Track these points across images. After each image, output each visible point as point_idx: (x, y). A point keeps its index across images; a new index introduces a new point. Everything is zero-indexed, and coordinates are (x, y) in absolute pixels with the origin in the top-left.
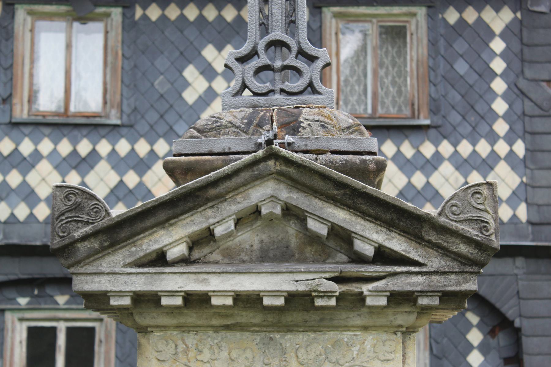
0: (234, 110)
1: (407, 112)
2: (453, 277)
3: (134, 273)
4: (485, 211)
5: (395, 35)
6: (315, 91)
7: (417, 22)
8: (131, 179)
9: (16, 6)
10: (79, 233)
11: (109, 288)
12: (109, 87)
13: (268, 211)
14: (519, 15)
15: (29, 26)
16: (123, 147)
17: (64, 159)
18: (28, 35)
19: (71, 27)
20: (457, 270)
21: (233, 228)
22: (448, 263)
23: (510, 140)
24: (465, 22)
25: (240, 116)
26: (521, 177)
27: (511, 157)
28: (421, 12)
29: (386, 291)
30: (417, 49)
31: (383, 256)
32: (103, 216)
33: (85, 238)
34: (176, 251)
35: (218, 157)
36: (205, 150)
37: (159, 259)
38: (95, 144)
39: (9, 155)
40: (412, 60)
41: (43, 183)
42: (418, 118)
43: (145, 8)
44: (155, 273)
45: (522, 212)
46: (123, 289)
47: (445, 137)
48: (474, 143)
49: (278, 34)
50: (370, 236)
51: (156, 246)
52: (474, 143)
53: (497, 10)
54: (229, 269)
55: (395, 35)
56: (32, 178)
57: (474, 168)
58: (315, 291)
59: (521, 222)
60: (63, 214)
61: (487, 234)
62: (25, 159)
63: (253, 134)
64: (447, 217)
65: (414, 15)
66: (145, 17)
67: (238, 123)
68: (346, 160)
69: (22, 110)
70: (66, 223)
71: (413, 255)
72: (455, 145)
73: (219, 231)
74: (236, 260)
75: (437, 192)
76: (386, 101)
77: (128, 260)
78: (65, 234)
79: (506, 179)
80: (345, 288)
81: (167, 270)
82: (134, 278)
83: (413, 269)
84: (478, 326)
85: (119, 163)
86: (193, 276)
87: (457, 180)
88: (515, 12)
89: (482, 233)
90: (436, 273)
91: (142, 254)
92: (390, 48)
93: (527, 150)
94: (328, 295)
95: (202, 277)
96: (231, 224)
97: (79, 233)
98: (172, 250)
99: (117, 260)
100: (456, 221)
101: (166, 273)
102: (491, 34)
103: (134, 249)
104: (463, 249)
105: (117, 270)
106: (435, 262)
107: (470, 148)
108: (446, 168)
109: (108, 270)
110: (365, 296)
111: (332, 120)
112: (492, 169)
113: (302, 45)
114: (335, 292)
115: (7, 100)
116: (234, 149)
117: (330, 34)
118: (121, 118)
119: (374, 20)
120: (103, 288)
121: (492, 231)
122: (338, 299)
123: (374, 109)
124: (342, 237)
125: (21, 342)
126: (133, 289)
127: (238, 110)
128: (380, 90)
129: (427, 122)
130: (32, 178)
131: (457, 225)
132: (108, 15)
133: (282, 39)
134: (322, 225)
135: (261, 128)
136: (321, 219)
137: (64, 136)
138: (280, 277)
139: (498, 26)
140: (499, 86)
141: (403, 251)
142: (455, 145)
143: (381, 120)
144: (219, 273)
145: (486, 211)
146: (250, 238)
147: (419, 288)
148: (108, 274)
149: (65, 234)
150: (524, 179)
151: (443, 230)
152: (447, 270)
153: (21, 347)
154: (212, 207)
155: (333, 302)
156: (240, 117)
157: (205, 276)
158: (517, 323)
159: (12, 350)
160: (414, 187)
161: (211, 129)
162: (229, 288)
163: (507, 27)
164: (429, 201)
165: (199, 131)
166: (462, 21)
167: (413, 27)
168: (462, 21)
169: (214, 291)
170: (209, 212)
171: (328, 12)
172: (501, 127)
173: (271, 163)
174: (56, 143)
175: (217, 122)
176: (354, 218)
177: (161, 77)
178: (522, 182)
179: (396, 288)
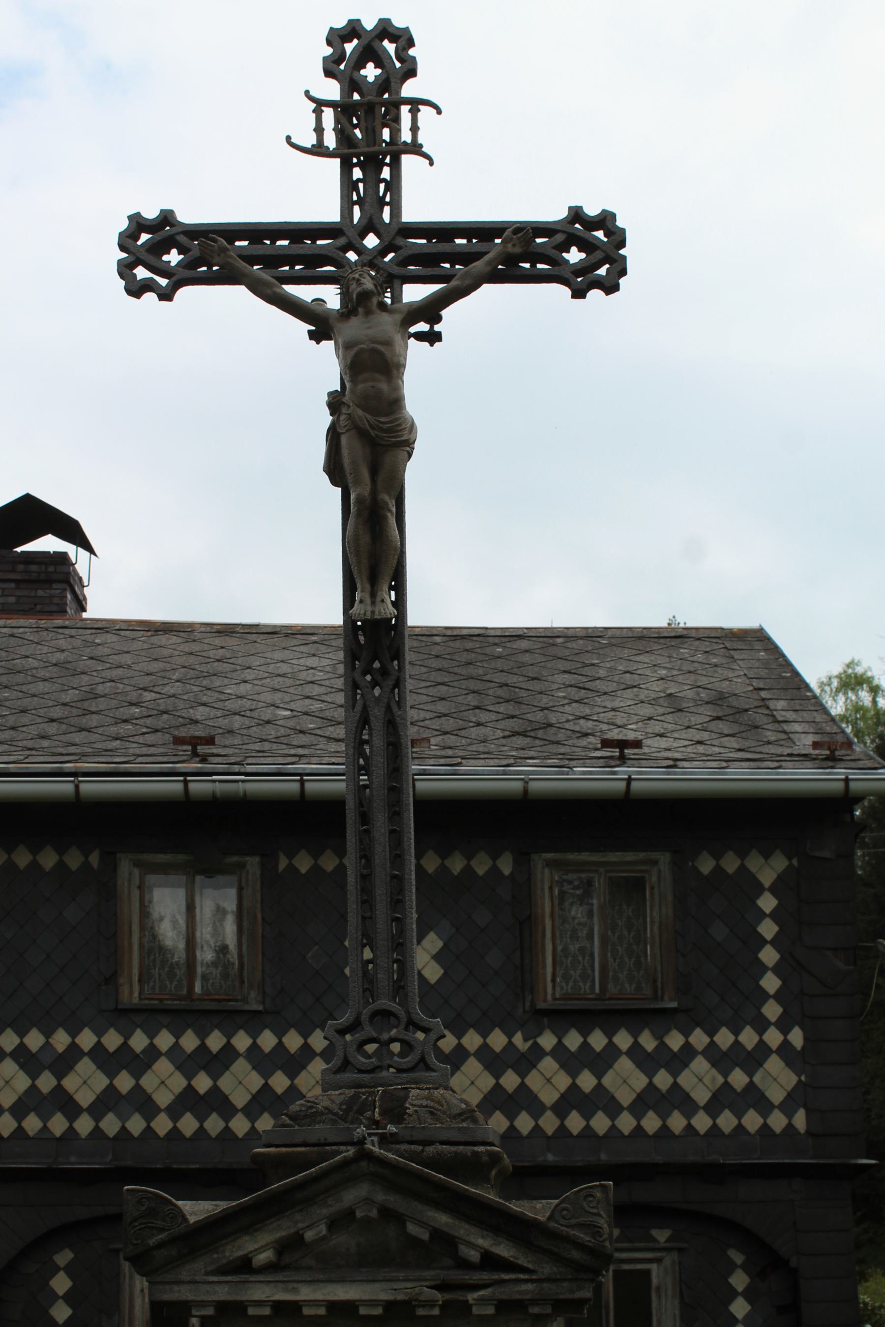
0: (333, 1093)
1: (647, 991)
2: (565, 1284)
3: (216, 1282)
4: (599, 1215)
5: (631, 889)
6: (429, 1068)
7: (660, 871)
8: (280, 1082)
9: (119, 855)
10: (154, 1240)
11: (191, 1297)
12: (245, 960)
13: (362, 1214)
14: (795, 862)
15: (137, 882)
16: (267, 1040)
17: (189, 1055)
18: (136, 893)
19: (193, 882)
20: (570, 1277)
21: (324, 1232)
22: (561, 1269)
23: (784, 1026)
24: (724, 871)
25: (339, 1100)
26: (799, 1075)
27: (785, 1050)
28: (664, 858)
29: (493, 1300)
30: (658, 910)
31: (490, 1261)
32: (180, 1221)
33: (160, 1245)
34: (265, 1257)
35: (311, 1148)
36: (298, 1139)
37: (244, 1266)
38: (229, 1037)
39: (115, 1052)
40: (652, 922)
41: (163, 1088)
42: (662, 999)
43: (290, 856)
44: (240, 1282)
45: (800, 1120)
46: (204, 1298)
47: (698, 1025)
48: (736, 1032)
49: (384, 1003)
50: (477, 1241)
51: (240, 1253)
52: (736, 1032)
53: (767, 856)
54: (321, 1277)
55: (631, 889)
56: (148, 1082)
57: (737, 1065)
58: (415, 1300)
59: (799, 1133)
60: (135, 1220)
61: (601, 1239)
62: (138, 1055)
63: (352, 1123)
64: (557, 1222)
65: (655, 863)
66: (291, 868)
67: (336, 1109)
68: (456, 1152)
69: (131, 993)
70: (140, 1229)
71: (522, 1261)
72: (711, 1033)
73: (309, 1235)
74: (331, 1267)
75: (687, 1096)
76: (620, 975)
77: (210, 1268)
78: (139, 1242)
79: (778, 1079)
80: (448, 1296)
81: (252, 1278)
82: (217, 1288)
83: (522, 1276)
84: (744, 1267)
85: (261, 1061)
86: (281, 1285)
87: (714, 1079)
88: (790, 859)
89: (595, 1239)
90: (548, 1280)
91: (224, 1261)
92: (625, 907)
93: (806, 1039)
94: (430, 1304)
95: (291, 1286)
96: (323, 1229)
97: (154, 1240)
98: (258, 1257)
99: (197, 1268)
100: (567, 1226)
101: (252, 1282)
102: (759, 889)
103: (215, 1256)
104: (575, 1255)
105: (198, 1278)
106: (547, 1269)
107: (731, 1038)
108: (700, 1064)
109: (188, 1279)
110: (471, 1305)
111: (442, 1106)
112: (760, 1065)
113: (413, 1015)
114: (437, 1301)
115: (111, 979)
116: (331, 1139)
117: (543, 889)
118: (263, 1003)
119: (602, 870)
120: (184, 1298)
121: (606, 1236)
122: (443, 1307)
123: (603, 988)
124: (445, 1242)
125: (142, 1290)
126: (215, 1298)
127: (337, 1092)
128: (611, 960)
129: (674, 1005)
130: (148, 1082)
131: (568, 1230)
132: (242, 866)
133: (389, 1009)
134: (423, 1230)
135: (362, 1115)
136: (422, 1224)
137: (189, 1026)
138: (377, 1286)
139: (767, 877)
140: (769, 956)
141: (511, 1256)
142: (711, 1033)
143: (612, 1002)
144: (310, 1281)
145: (599, 1215)
146: (344, 1241)
147: (529, 1297)
148: (189, 1282)
149: (139, 1242)
150: (803, 1078)
151: (555, 1236)
152: (558, 1277)
153: (144, 1297)
154: (301, 1210)
155: (436, 1311)
156: (338, 1102)
157: (295, 1285)
158: (793, 1263)
159: (131, 1300)
160: (656, 1089)
161: (306, 1116)
162: (321, 1297)
163: (779, 877)
164: (677, 1108)
165: (291, 1118)
166: (718, 870)
167: (654, 879)
168: (718, 870)
169: (305, 1301)
170: (298, 1217)
171: (539, 860)
172: (772, 1011)
173: (364, 1164)
174: (177, 1036)
175: (312, 1107)
176: (457, 1223)
177: (316, 947)
178: (800, 1081)
179: (504, 1297)
